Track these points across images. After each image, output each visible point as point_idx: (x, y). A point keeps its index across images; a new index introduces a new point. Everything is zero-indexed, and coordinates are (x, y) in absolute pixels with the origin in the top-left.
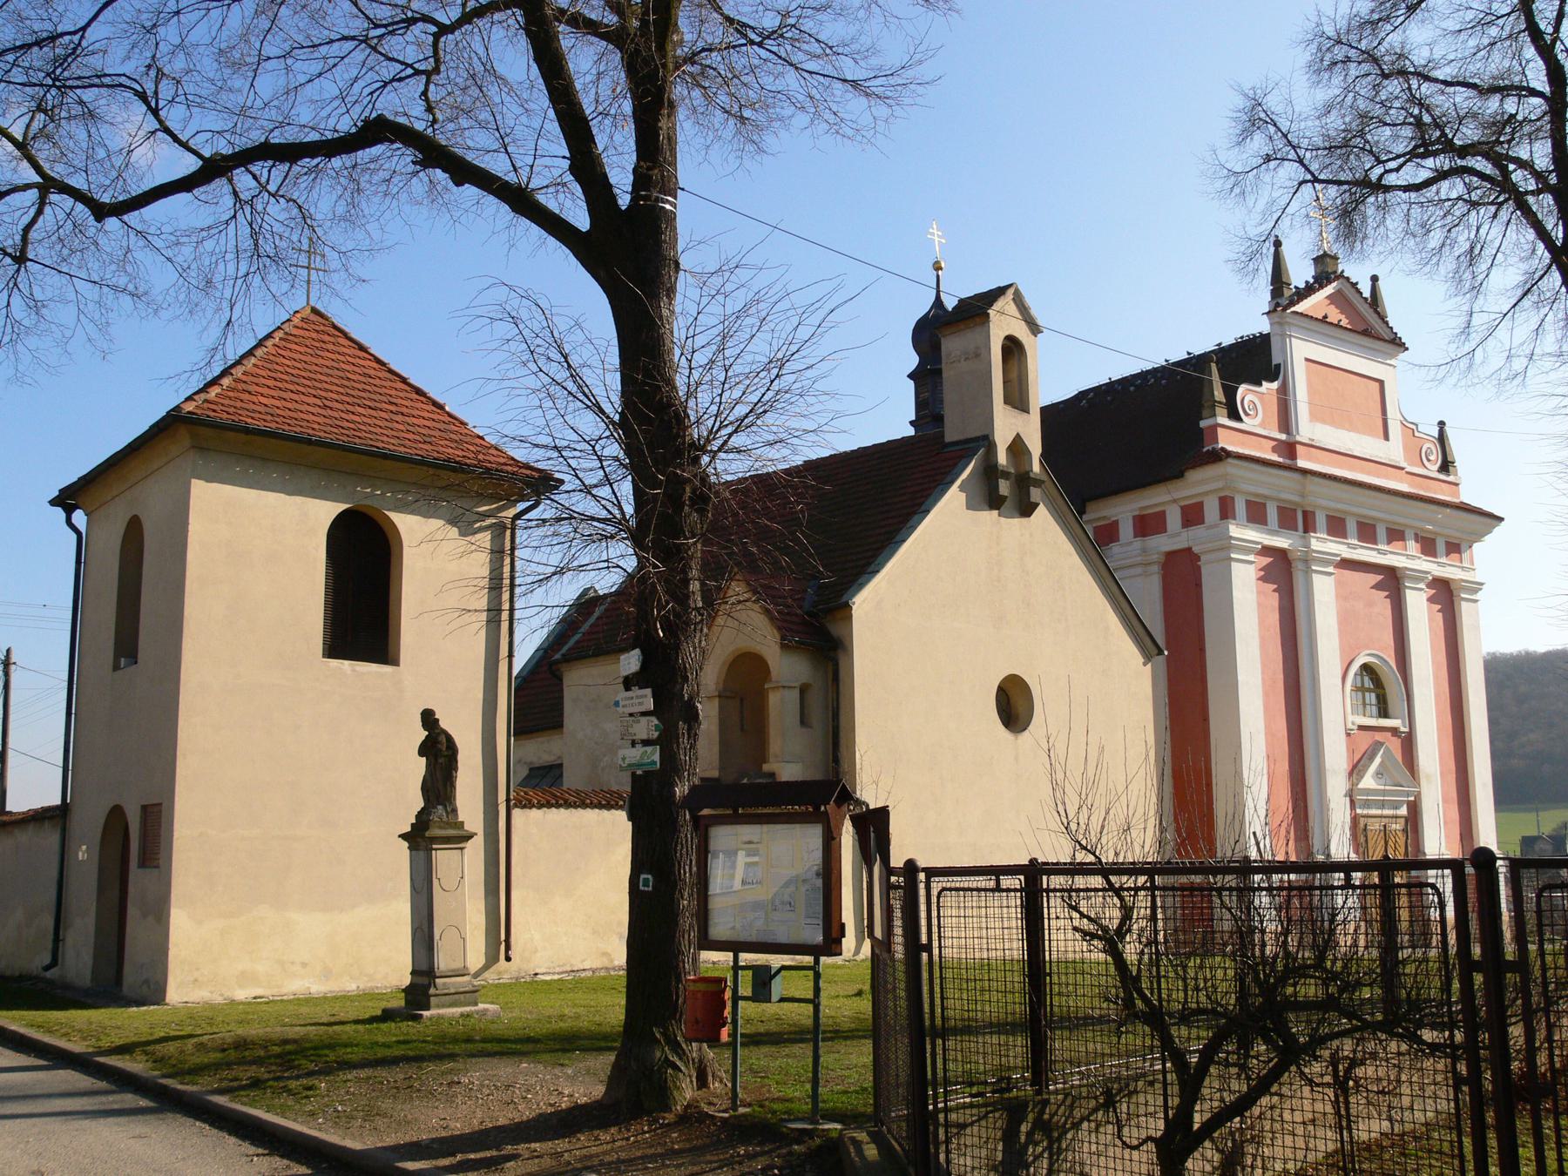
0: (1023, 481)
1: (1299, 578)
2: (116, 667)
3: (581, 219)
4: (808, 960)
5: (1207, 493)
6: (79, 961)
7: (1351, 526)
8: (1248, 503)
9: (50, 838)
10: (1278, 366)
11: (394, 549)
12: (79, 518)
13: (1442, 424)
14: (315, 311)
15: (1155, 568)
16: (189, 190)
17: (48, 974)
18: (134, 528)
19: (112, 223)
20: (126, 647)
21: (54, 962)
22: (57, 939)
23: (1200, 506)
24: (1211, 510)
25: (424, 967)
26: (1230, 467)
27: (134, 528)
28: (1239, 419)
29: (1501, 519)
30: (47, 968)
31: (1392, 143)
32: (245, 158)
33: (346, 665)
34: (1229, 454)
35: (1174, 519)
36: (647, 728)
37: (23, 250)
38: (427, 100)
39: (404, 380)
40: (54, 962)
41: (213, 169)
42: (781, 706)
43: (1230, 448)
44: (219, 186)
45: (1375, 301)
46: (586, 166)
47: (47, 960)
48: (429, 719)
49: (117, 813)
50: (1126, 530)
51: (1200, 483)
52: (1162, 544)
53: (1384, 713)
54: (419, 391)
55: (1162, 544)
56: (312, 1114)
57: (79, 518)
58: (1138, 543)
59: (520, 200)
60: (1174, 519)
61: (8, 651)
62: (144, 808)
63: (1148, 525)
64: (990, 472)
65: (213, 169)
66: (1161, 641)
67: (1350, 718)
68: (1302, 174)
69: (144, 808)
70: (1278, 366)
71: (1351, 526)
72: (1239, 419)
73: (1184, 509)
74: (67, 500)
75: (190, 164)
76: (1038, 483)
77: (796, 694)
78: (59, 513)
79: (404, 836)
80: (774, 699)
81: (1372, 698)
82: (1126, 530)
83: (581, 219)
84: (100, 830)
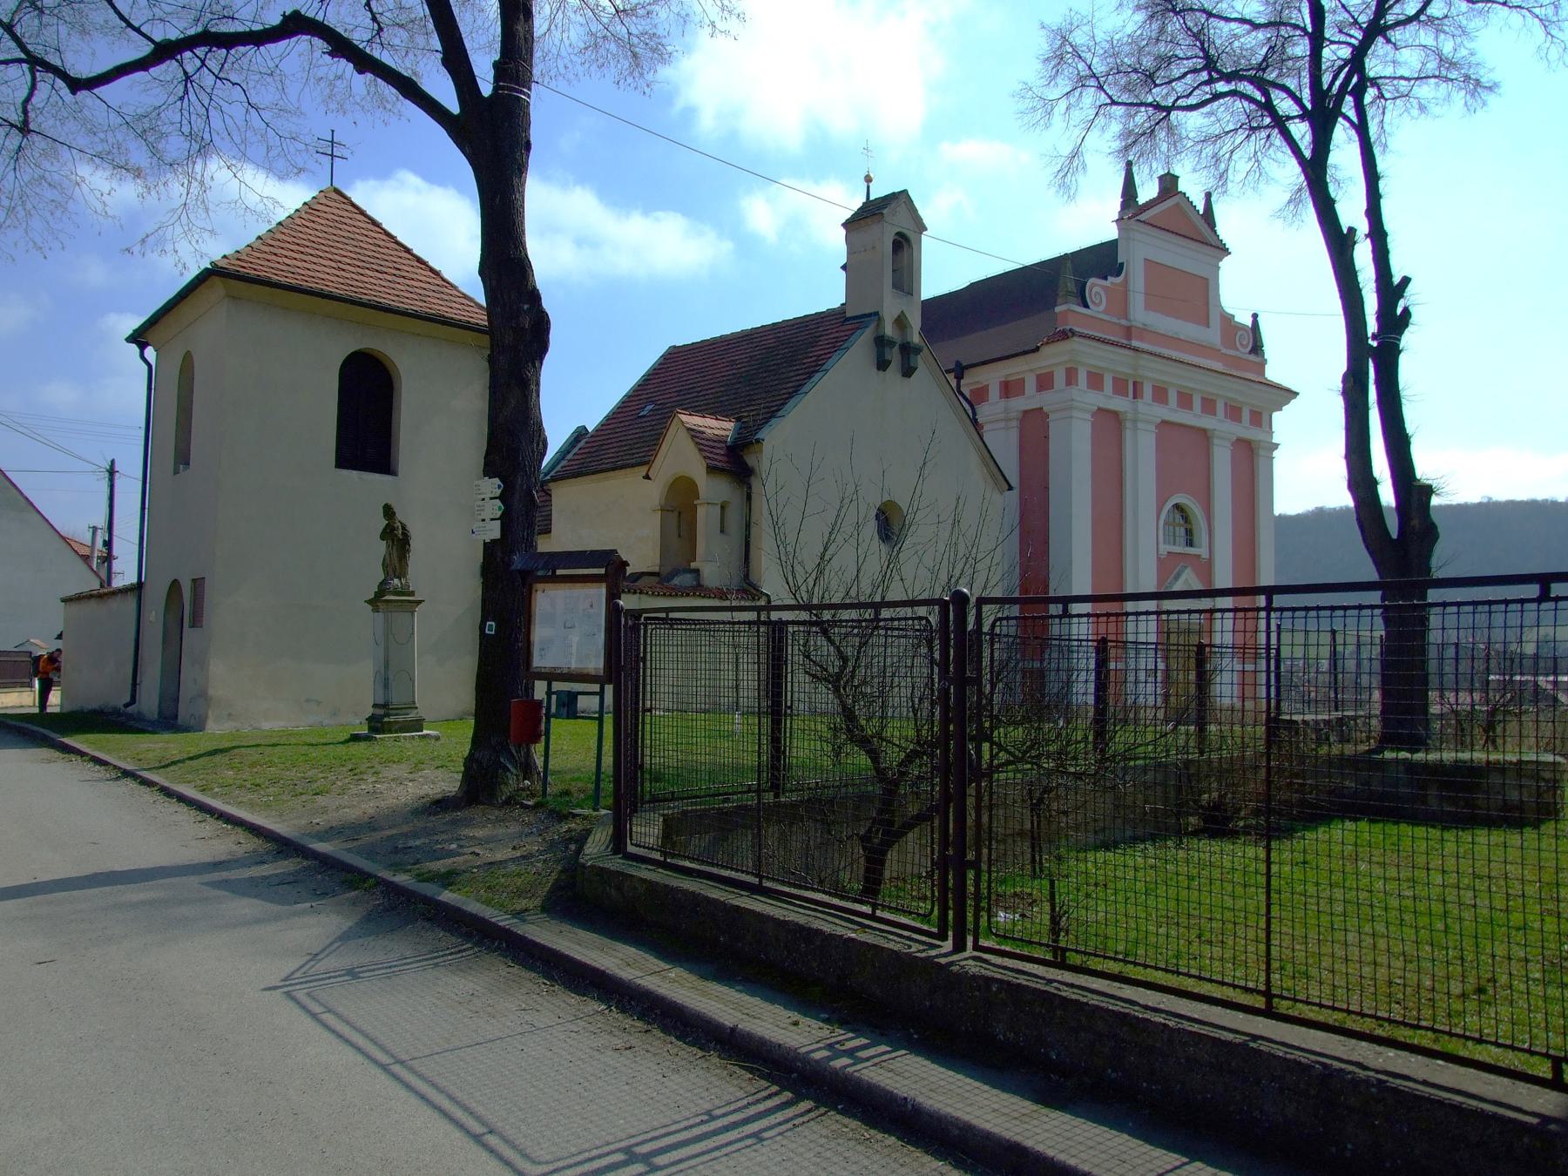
0: (907, 350)
1: (1128, 434)
2: (176, 472)
3: (454, 107)
4: (596, 688)
5: (1057, 364)
6: (149, 702)
7: (1197, 403)
8: (1089, 373)
9: (130, 603)
10: (1122, 265)
11: (396, 386)
12: (150, 353)
13: (1255, 316)
14: (337, 191)
15: (1015, 423)
16: (146, 69)
17: (130, 709)
18: (188, 360)
19: (83, 95)
20: (183, 458)
21: (133, 700)
22: (134, 684)
23: (1051, 375)
24: (1060, 378)
25: (381, 701)
26: (1075, 344)
27: (188, 360)
28: (1086, 306)
29: (1296, 394)
30: (126, 705)
31: (1161, 72)
32: (189, 43)
33: (354, 474)
34: (1073, 333)
35: (1030, 385)
36: (496, 508)
37: (26, 122)
38: (371, 10)
39: (408, 251)
40: (133, 700)
41: (165, 51)
42: (706, 517)
43: (1077, 329)
44: (168, 70)
45: (1209, 216)
46: (456, 60)
47: (128, 699)
48: (388, 511)
49: (175, 586)
50: (994, 392)
51: (1053, 357)
52: (1020, 404)
53: (1190, 543)
54: (419, 260)
55: (1020, 404)
56: (268, 806)
57: (150, 353)
58: (1003, 403)
59: (409, 89)
60: (1030, 385)
61: (113, 462)
62: (194, 581)
63: (1010, 389)
64: (881, 342)
65: (165, 51)
66: (1014, 481)
67: (1162, 546)
68: (1104, 99)
69: (194, 581)
70: (1122, 265)
71: (1220, 407)
72: (1086, 306)
73: (1038, 377)
74: (139, 338)
75: (145, 49)
76: (918, 350)
77: (718, 509)
78: (134, 348)
79: (370, 602)
80: (701, 512)
81: (1181, 531)
82: (994, 392)
83: (454, 107)
84: (164, 595)
